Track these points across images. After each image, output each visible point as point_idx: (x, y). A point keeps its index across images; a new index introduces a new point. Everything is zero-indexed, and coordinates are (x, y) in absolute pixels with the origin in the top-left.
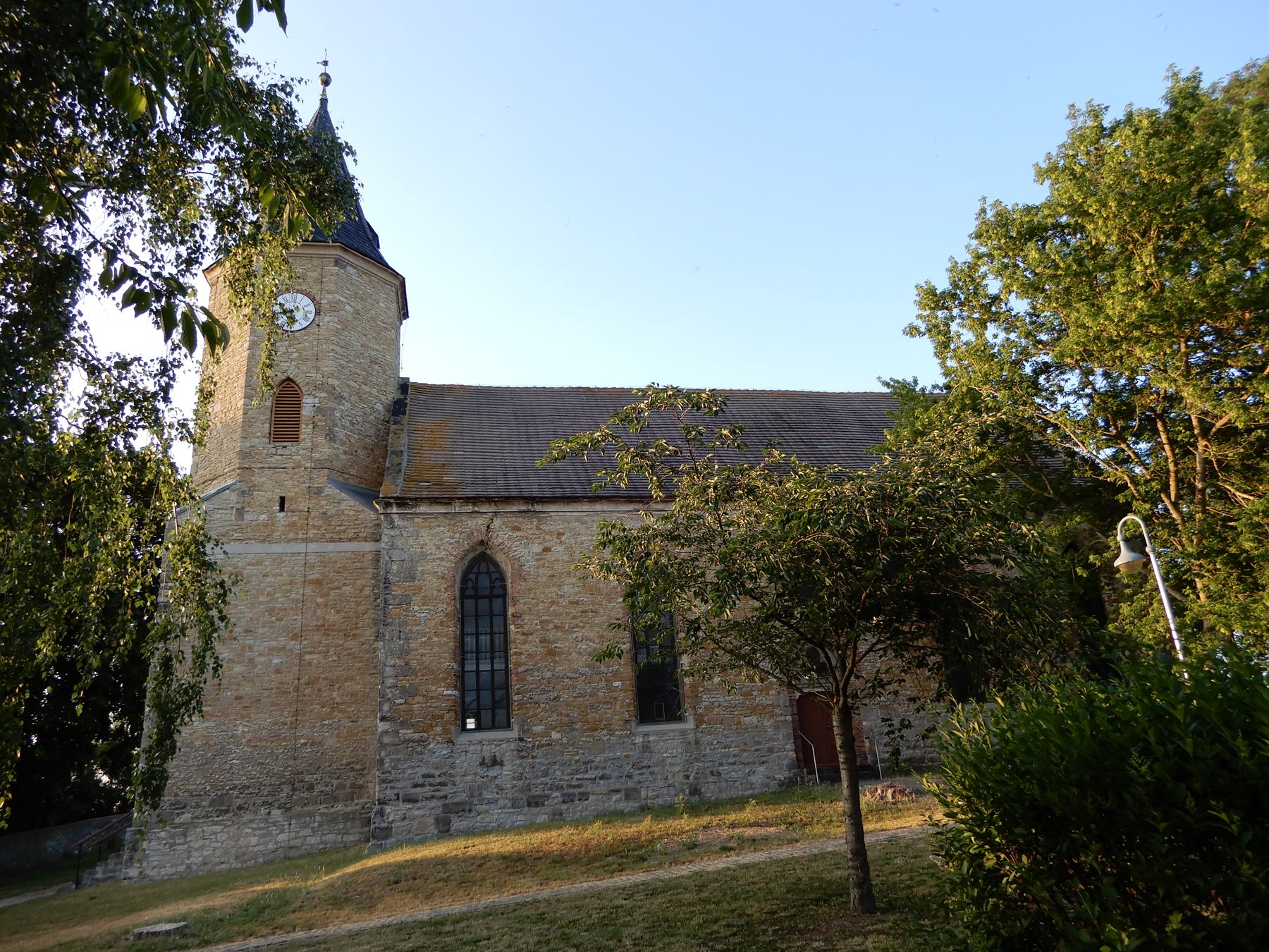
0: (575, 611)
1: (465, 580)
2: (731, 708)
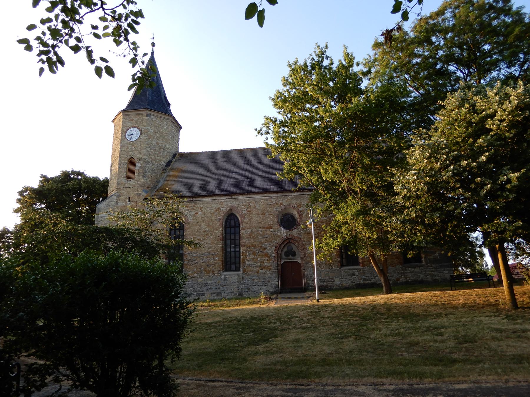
0: (204, 234)
1: (226, 222)
2: (256, 267)
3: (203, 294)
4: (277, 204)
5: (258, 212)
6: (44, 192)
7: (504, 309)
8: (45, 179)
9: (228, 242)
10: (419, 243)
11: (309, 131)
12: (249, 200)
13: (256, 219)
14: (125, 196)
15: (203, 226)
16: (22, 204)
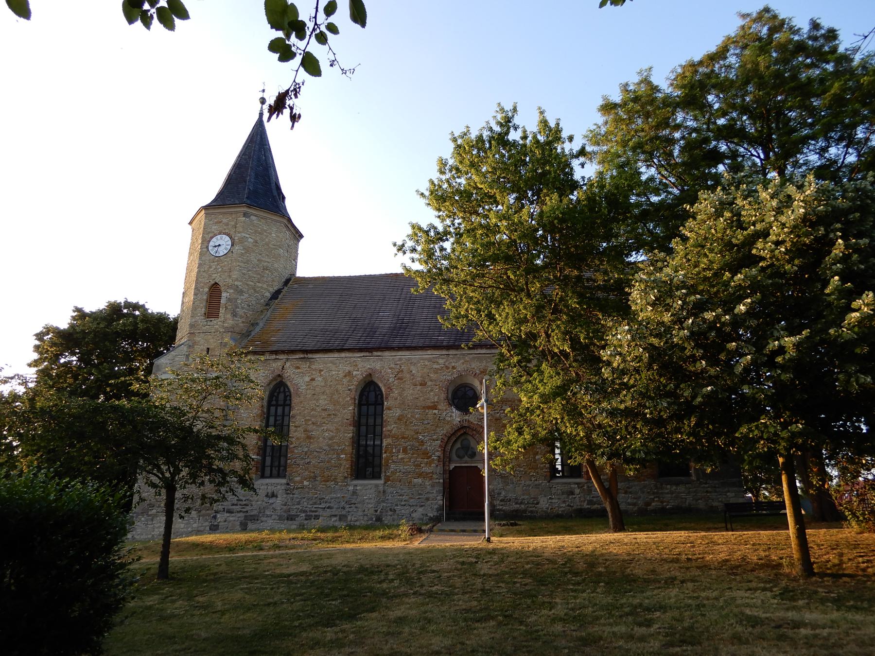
0: (324, 414)
2: (407, 473)
3: (316, 516)
4: (447, 368)
5: (413, 379)
6: (75, 336)
7: (787, 576)
8: (81, 315)
9: (363, 429)
10: (634, 452)
11: (476, 250)
12: (400, 359)
13: (410, 393)
14: (200, 349)
15: (323, 401)
16: (41, 353)
